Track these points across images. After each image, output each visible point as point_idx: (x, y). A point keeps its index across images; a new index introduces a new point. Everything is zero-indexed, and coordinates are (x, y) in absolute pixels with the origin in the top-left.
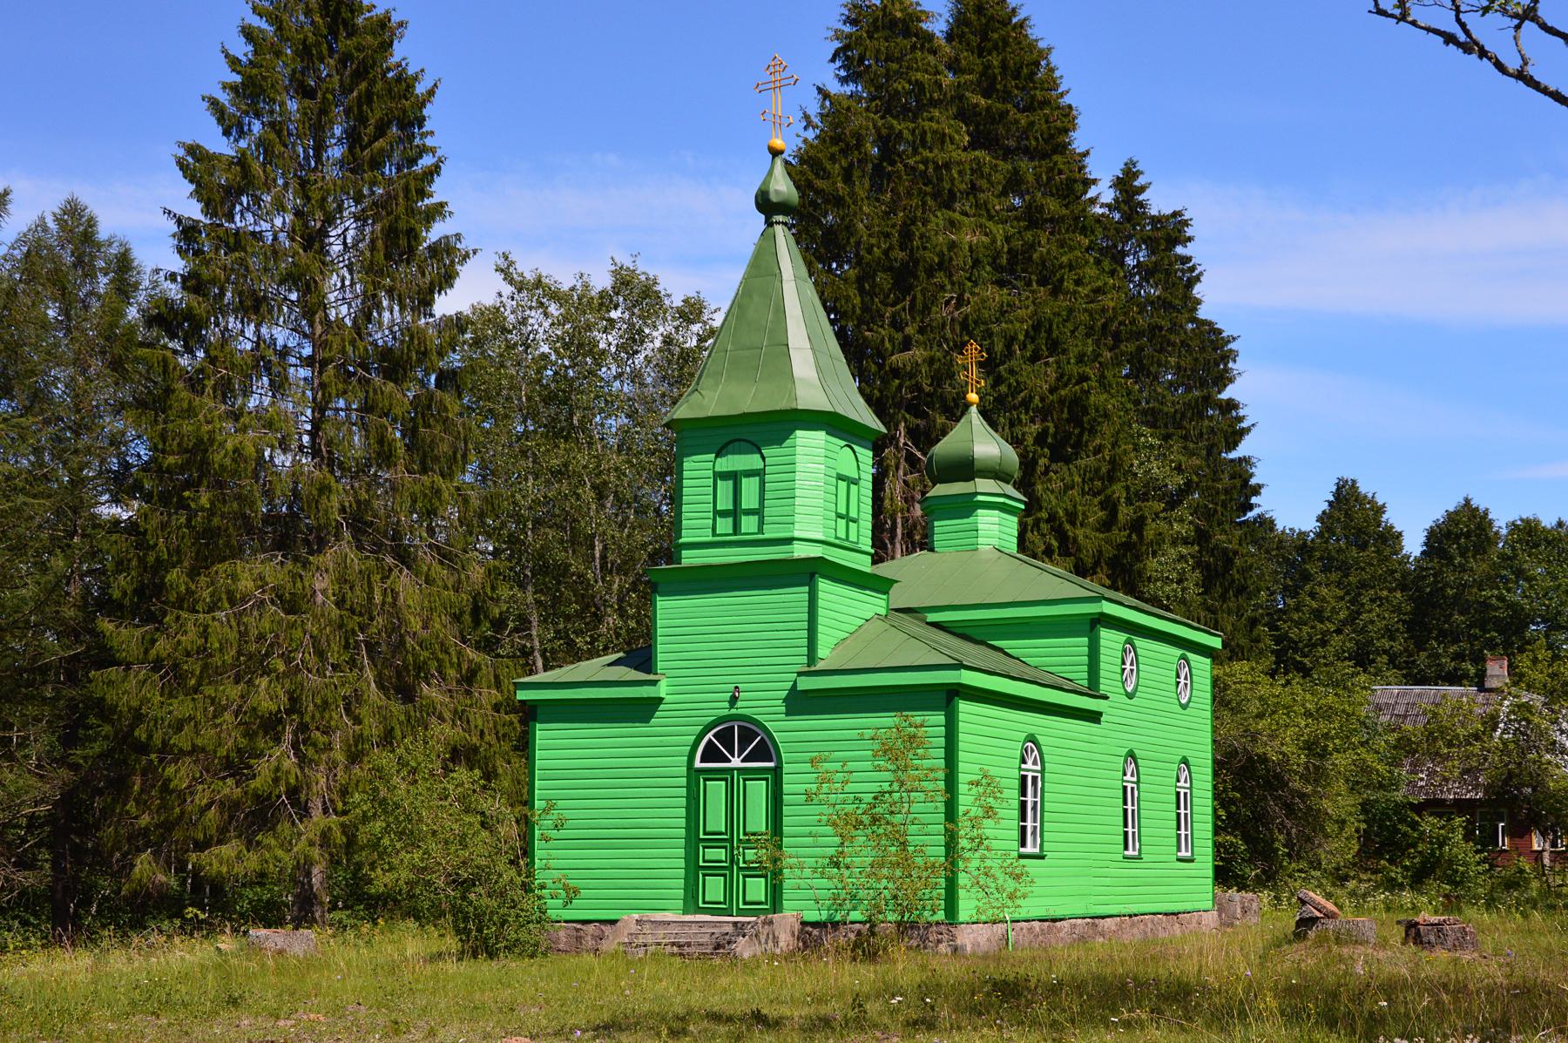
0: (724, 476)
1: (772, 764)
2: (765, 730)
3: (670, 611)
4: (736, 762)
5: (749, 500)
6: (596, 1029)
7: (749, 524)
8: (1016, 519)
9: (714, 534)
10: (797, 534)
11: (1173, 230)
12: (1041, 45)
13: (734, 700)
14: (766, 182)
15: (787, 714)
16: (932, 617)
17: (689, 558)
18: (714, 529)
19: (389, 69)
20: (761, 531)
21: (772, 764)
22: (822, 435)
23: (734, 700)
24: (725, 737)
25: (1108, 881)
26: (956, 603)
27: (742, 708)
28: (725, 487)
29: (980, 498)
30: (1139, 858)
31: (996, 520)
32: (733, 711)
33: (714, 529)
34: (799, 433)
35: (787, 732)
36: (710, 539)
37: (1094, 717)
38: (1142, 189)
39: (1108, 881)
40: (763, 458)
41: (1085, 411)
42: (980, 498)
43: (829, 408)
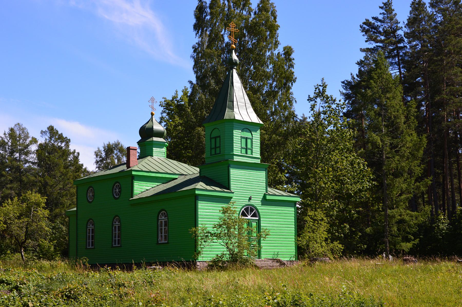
0: (244, 138)
1: (257, 218)
2: (257, 210)
3: (234, 173)
4: (249, 217)
6: (75, 298)
13: (250, 199)
15: (262, 205)
17: (236, 159)
19: (381, 41)
20: (252, 154)
21: (257, 218)
23: (250, 199)
24: (247, 209)
27: (252, 202)
28: (244, 140)
30: (121, 246)
32: (249, 203)
35: (263, 210)
36: (240, 154)
40: (252, 134)
43: (251, 121)
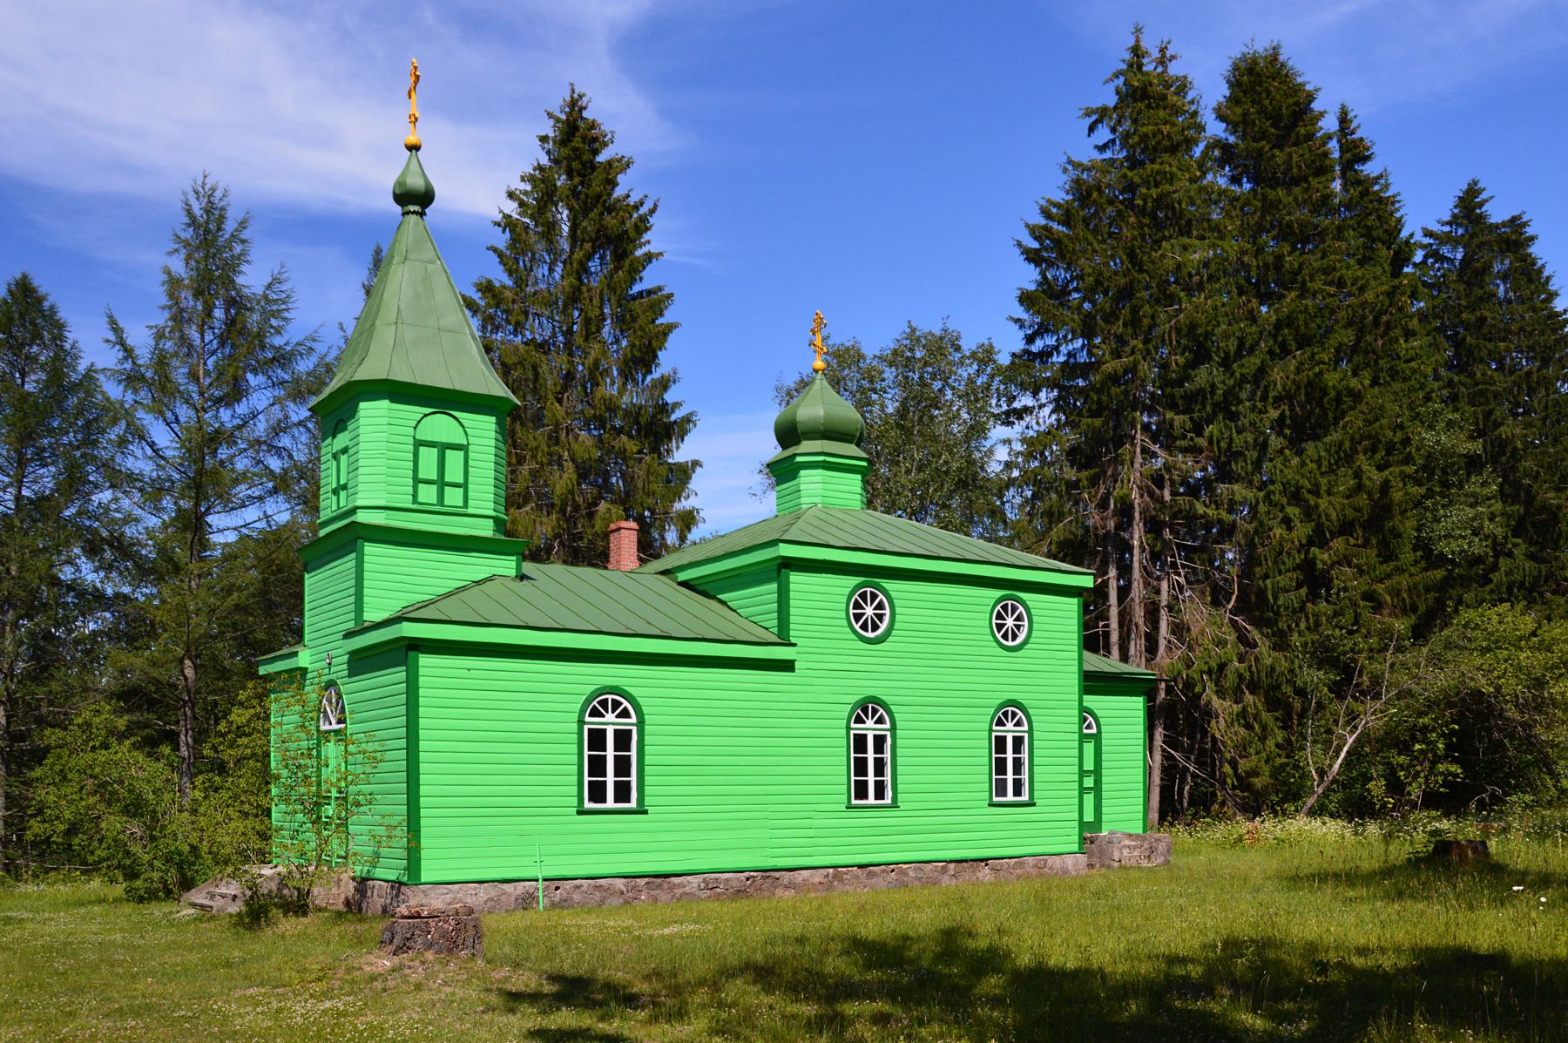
5: (454, 473)
7: (453, 497)
8: (859, 477)
9: (415, 501)
10: (359, 503)
11: (1514, 238)
12: (1308, 87)
14: (404, 173)
16: (682, 576)
18: (415, 495)
22: (385, 403)
25: (811, 832)
26: (711, 555)
28: (429, 457)
29: (799, 459)
31: (819, 479)
33: (415, 495)
34: (362, 405)
37: (787, 666)
38: (1481, 205)
39: (811, 832)
41: (1324, 392)
42: (799, 459)
